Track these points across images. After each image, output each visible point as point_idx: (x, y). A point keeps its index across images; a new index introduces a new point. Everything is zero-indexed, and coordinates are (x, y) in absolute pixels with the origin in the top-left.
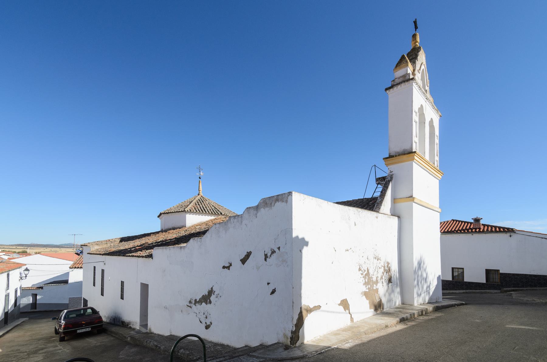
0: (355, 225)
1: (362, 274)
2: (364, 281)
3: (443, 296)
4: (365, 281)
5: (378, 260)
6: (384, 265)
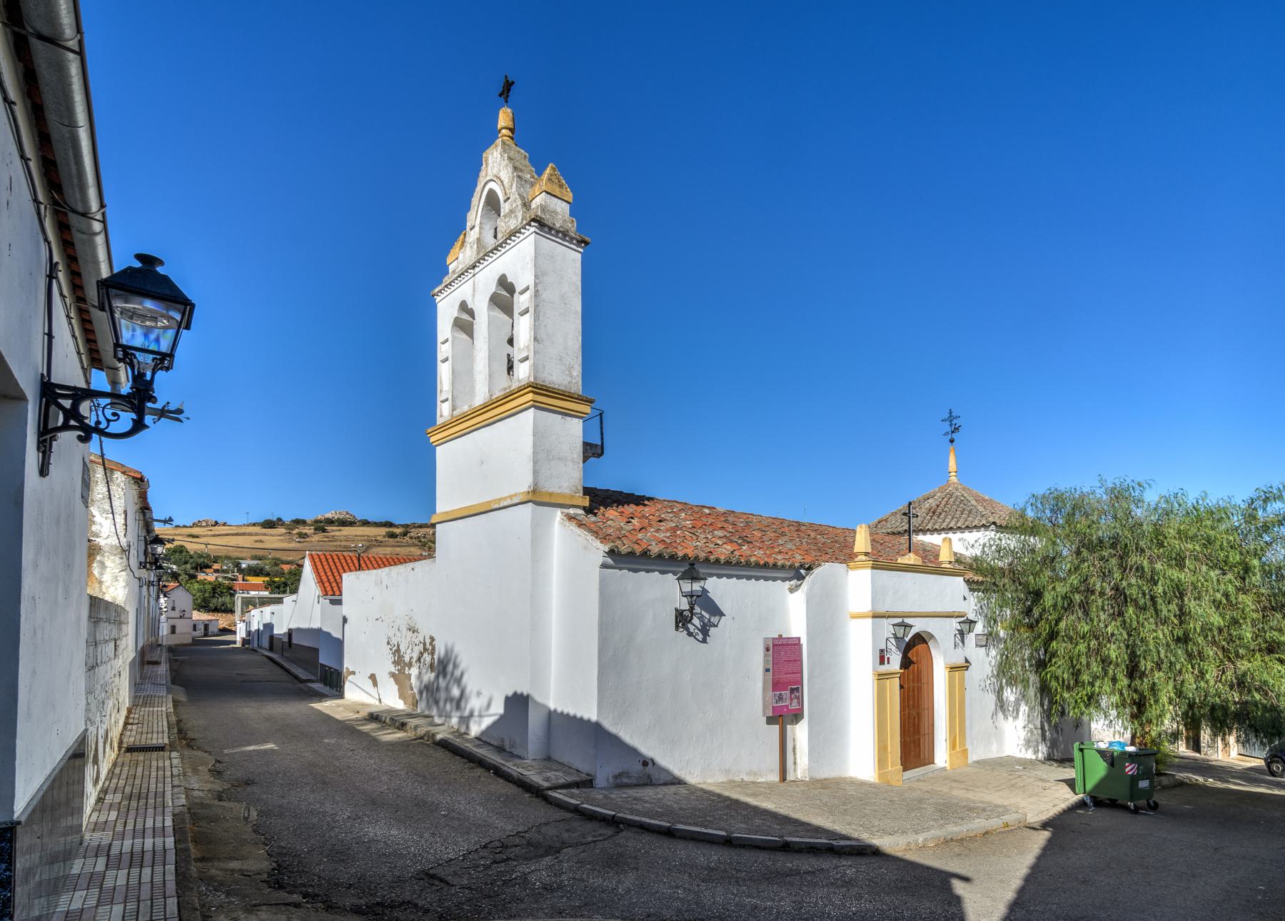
0: (387, 588)
1: (391, 649)
2: (393, 659)
3: (884, 664)
4: (395, 660)
5: (413, 632)
6: (424, 640)
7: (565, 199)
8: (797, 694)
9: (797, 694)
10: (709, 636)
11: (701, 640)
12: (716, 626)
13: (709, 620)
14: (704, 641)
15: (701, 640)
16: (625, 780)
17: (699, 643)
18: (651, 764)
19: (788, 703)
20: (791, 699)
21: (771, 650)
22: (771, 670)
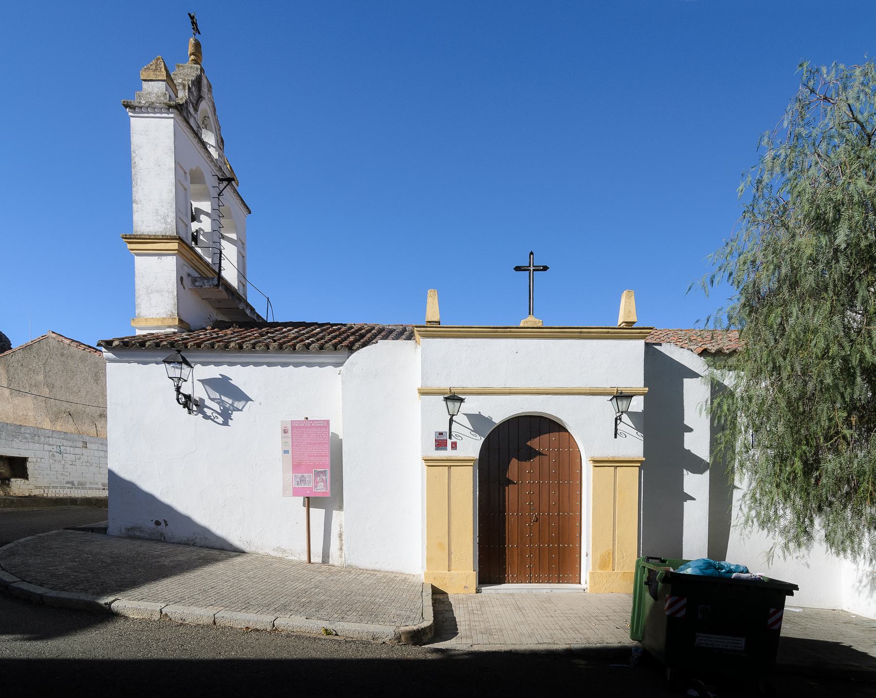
7: (160, 78)
8: (324, 478)
9: (324, 478)
10: (232, 419)
11: (222, 423)
12: (241, 410)
13: (232, 405)
14: (226, 423)
15: (222, 423)
16: (138, 534)
17: (448, 414)
18: (163, 524)
19: (312, 485)
20: (316, 483)
21: (290, 432)
22: (290, 452)
